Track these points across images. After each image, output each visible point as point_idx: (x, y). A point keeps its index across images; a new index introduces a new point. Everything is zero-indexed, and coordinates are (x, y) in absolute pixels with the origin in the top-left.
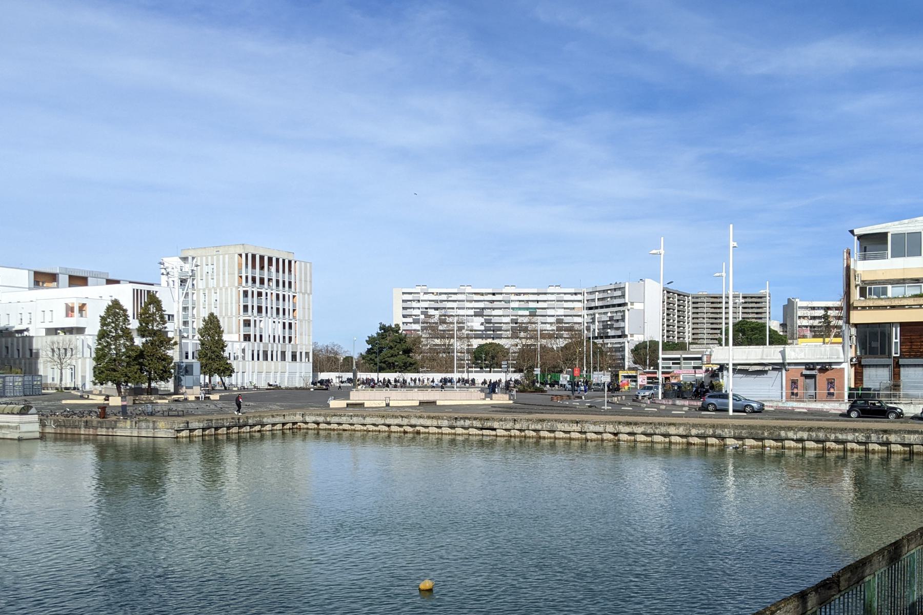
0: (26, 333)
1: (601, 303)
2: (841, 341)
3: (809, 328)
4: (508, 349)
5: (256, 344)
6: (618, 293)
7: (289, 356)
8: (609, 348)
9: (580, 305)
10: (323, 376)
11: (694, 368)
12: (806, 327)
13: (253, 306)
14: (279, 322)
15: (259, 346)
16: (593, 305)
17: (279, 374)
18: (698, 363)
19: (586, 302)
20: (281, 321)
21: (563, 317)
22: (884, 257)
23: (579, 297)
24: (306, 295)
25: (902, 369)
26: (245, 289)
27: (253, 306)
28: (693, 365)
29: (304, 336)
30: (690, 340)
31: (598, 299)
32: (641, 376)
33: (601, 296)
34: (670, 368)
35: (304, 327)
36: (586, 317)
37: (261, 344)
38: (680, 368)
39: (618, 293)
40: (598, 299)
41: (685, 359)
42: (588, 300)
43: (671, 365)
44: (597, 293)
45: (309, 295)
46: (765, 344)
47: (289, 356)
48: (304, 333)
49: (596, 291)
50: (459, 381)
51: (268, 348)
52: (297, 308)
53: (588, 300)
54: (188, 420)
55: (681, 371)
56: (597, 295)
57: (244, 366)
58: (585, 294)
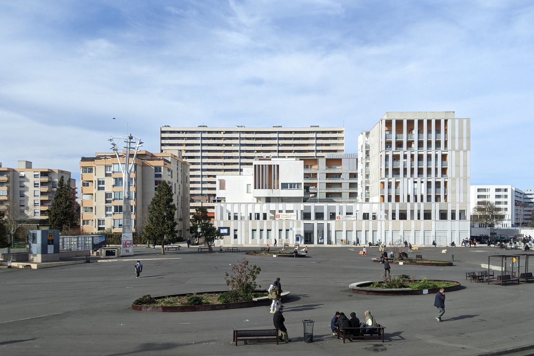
2: (69, 238)
4: (29, 216)
5: (390, 204)
7: (435, 215)
8: (202, 230)
13: (436, 169)
14: (422, 182)
15: (419, 206)
17: (421, 234)
20: (425, 181)
24: (462, 153)
25: (119, 171)
26: (444, 153)
27: (436, 169)
29: (457, 195)
30: (504, 223)
35: (457, 184)
37: (397, 204)
45: (465, 151)
47: (435, 215)
48: (457, 191)
50: (385, 286)
51: (407, 208)
52: (449, 167)
54: (259, 288)
57: (375, 226)
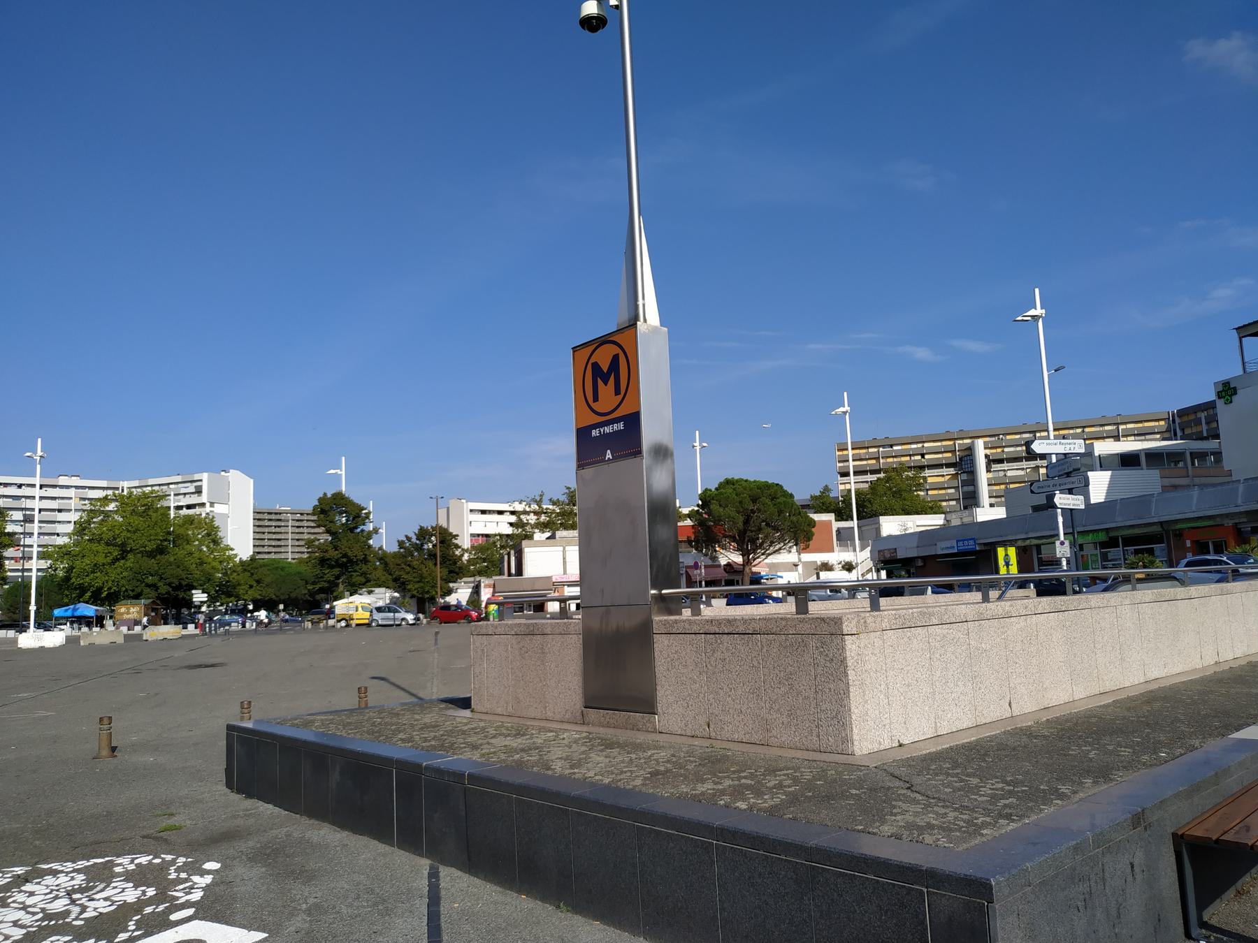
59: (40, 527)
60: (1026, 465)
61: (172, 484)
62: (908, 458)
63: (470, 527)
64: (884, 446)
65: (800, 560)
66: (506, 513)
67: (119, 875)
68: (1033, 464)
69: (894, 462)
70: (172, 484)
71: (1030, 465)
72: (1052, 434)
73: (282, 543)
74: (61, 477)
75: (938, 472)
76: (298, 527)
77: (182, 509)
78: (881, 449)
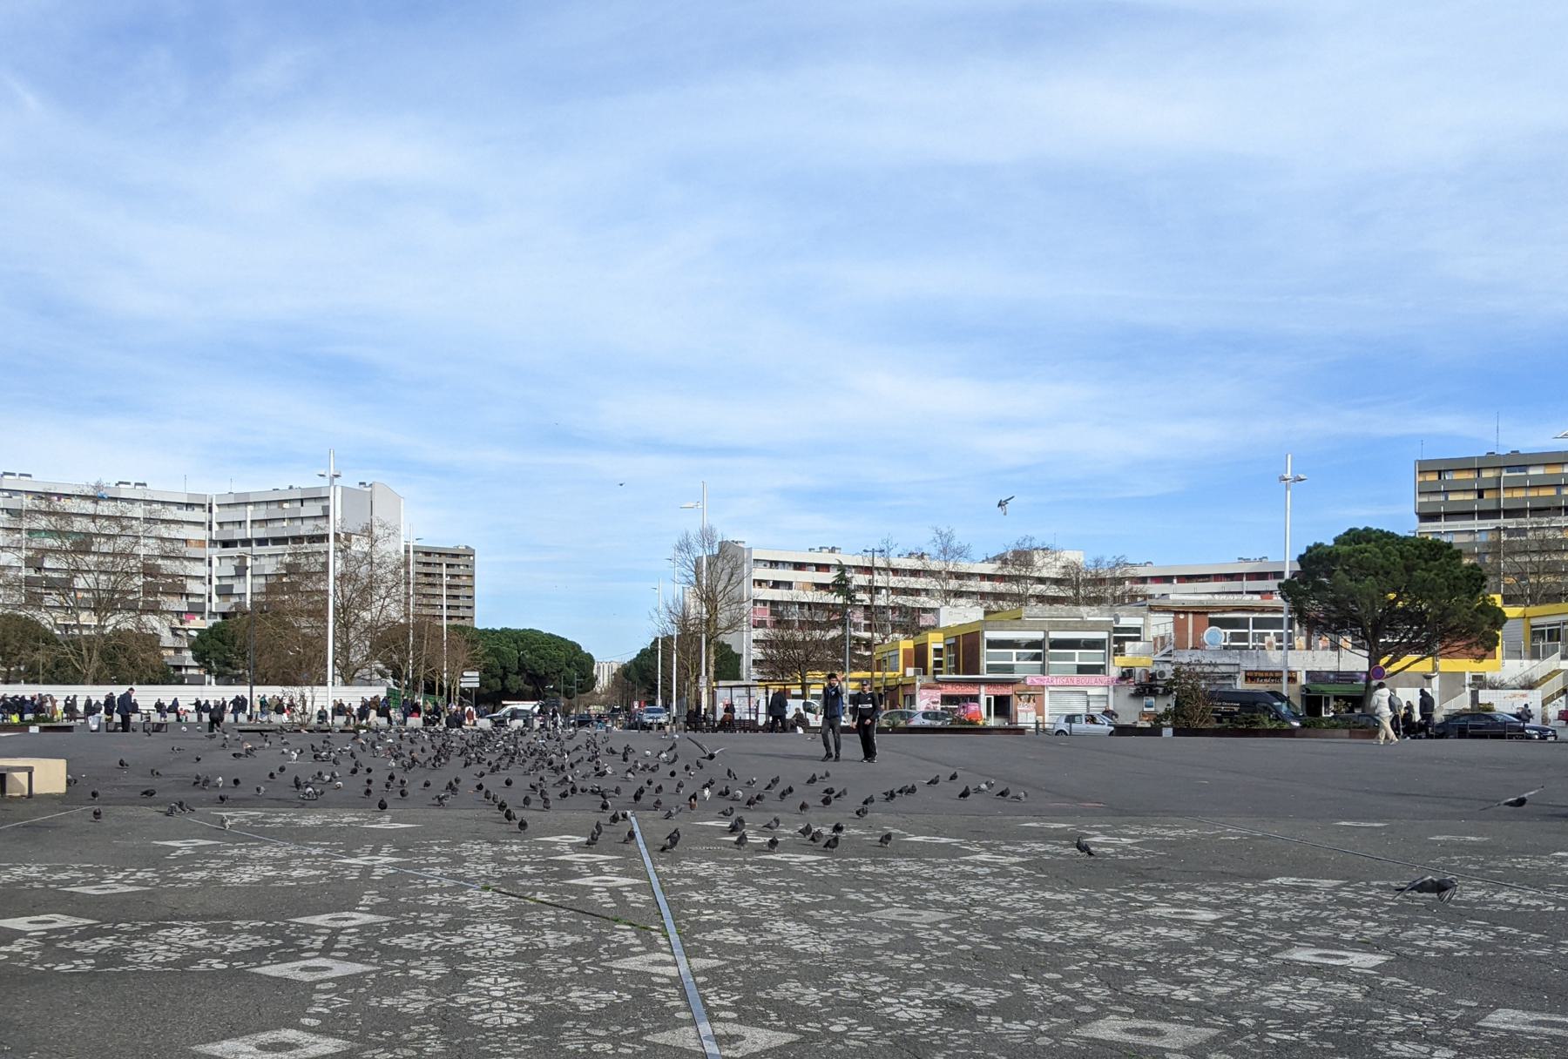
0: (741, 545)
1: (260, 533)
3: (768, 604)
6: (313, 509)
9: (201, 534)
10: (868, 653)
11: (1082, 670)
12: (764, 602)
16: (238, 534)
18: (1093, 657)
19: (215, 527)
21: (160, 562)
22: (1500, 518)
23: (198, 515)
28: (1077, 662)
31: (252, 521)
32: (924, 692)
33: (262, 513)
34: (1010, 669)
36: (215, 562)
38: (1043, 671)
39: (313, 509)
40: (252, 521)
41: (1057, 644)
42: (220, 524)
43: (1014, 662)
44: (250, 508)
46: (325, 684)
49: (250, 503)
53: (220, 524)
55: (1045, 680)
56: (250, 513)
58: (215, 509)
59: (417, 579)
60: (1479, 525)
61: (286, 501)
62: (1552, 492)
63: (34, 479)
64: (1509, 468)
65: (1435, 669)
66: (807, 568)
67: (90, 957)
68: (1492, 524)
69: (1525, 499)
70: (286, 501)
71: (1486, 525)
72: (41, 678)
73: (433, 601)
74: (6, 477)
75: (1462, 526)
76: (427, 575)
77: (919, 595)
78: (1505, 474)
